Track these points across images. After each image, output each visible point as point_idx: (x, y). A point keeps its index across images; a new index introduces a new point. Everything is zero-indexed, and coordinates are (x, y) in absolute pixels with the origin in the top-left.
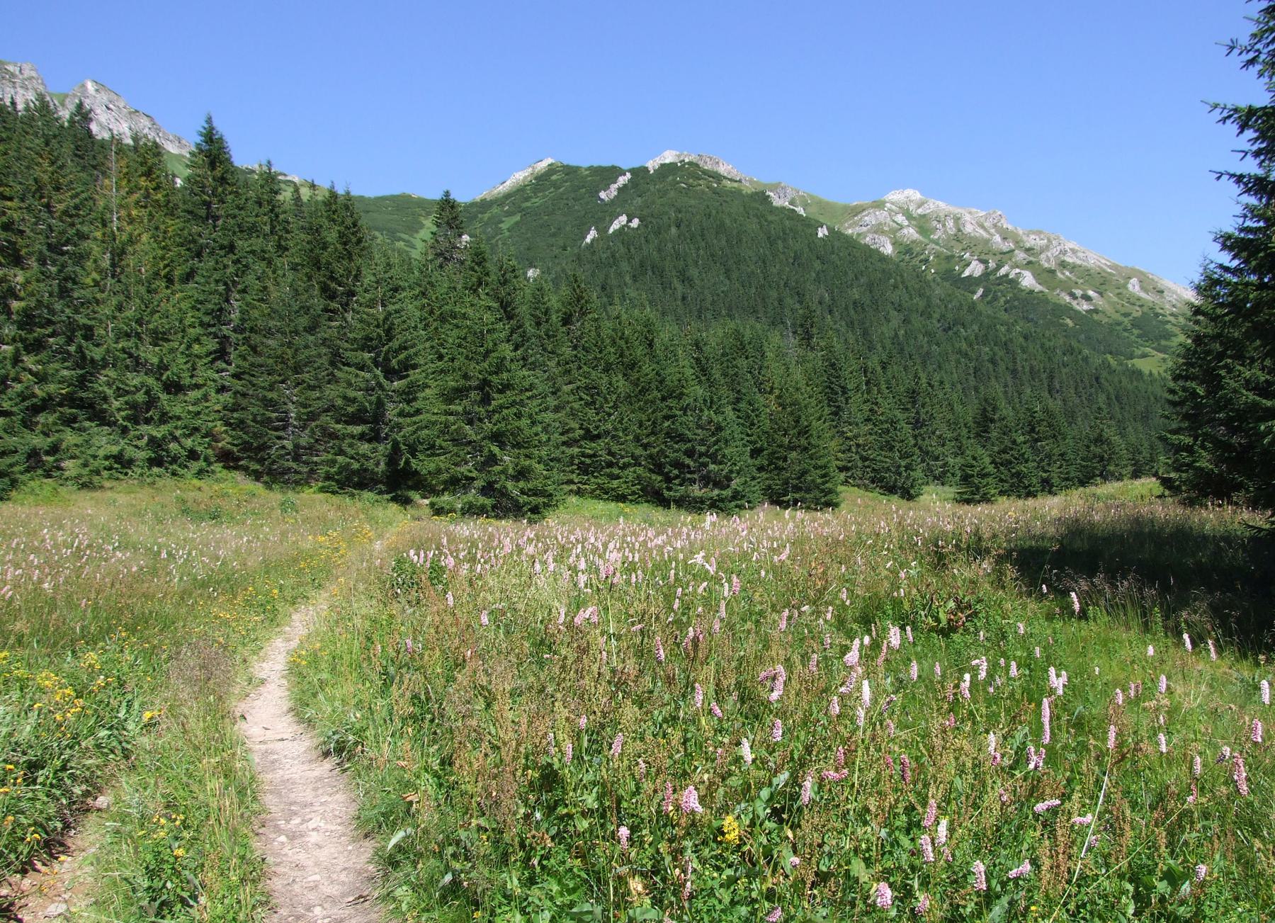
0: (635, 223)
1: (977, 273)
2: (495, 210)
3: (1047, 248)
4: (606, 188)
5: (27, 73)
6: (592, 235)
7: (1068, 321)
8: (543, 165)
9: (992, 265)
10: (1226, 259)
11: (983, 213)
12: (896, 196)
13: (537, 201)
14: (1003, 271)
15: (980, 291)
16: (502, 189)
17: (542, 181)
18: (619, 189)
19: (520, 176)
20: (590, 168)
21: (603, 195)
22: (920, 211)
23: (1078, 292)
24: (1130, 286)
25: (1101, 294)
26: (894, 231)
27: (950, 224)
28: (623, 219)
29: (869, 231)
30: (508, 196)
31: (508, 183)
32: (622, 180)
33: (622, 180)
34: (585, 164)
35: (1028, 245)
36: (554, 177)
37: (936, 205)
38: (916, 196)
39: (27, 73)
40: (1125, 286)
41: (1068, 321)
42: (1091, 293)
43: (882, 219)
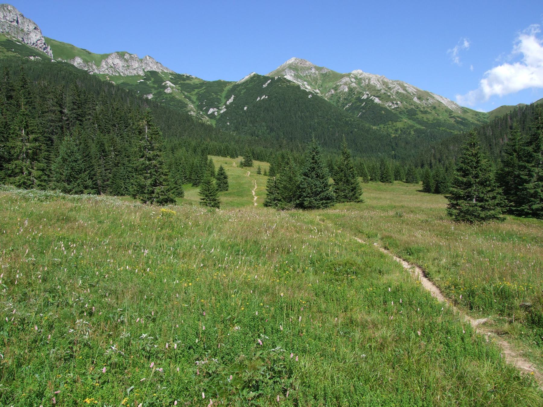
0: (267, 97)
1: (365, 98)
2: (240, 87)
3: (394, 87)
4: (265, 84)
5: (135, 57)
6: (259, 99)
7: (383, 112)
8: (252, 74)
9: (369, 95)
10: (102, 193)
11: (380, 76)
12: (354, 72)
13: (250, 86)
14: (371, 98)
15: (364, 103)
16: (243, 81)
17: (252, 79)
18: (268, 84)
19: (247, 77)
20: (263, 76)
21: (264, 86)
22: (360, 77)
23: (395, 102)
24: (414, 99)
25: (401, 102)
26: (350, 84)
27: (367, 81)
28: (264, 96)
29: (343, 84)
30: (244, 83)
31: (245, 78)
32: (269, 82)
33: (269, 82)
34: (262, 75)
35: (390, 87)
36: (255, 78)
37: (366, 75)
38: (360, 71)
39: (135, 57)
40: (412, 99)
41: (383, 112)
42: (399, 102)
43: (347, 80)
